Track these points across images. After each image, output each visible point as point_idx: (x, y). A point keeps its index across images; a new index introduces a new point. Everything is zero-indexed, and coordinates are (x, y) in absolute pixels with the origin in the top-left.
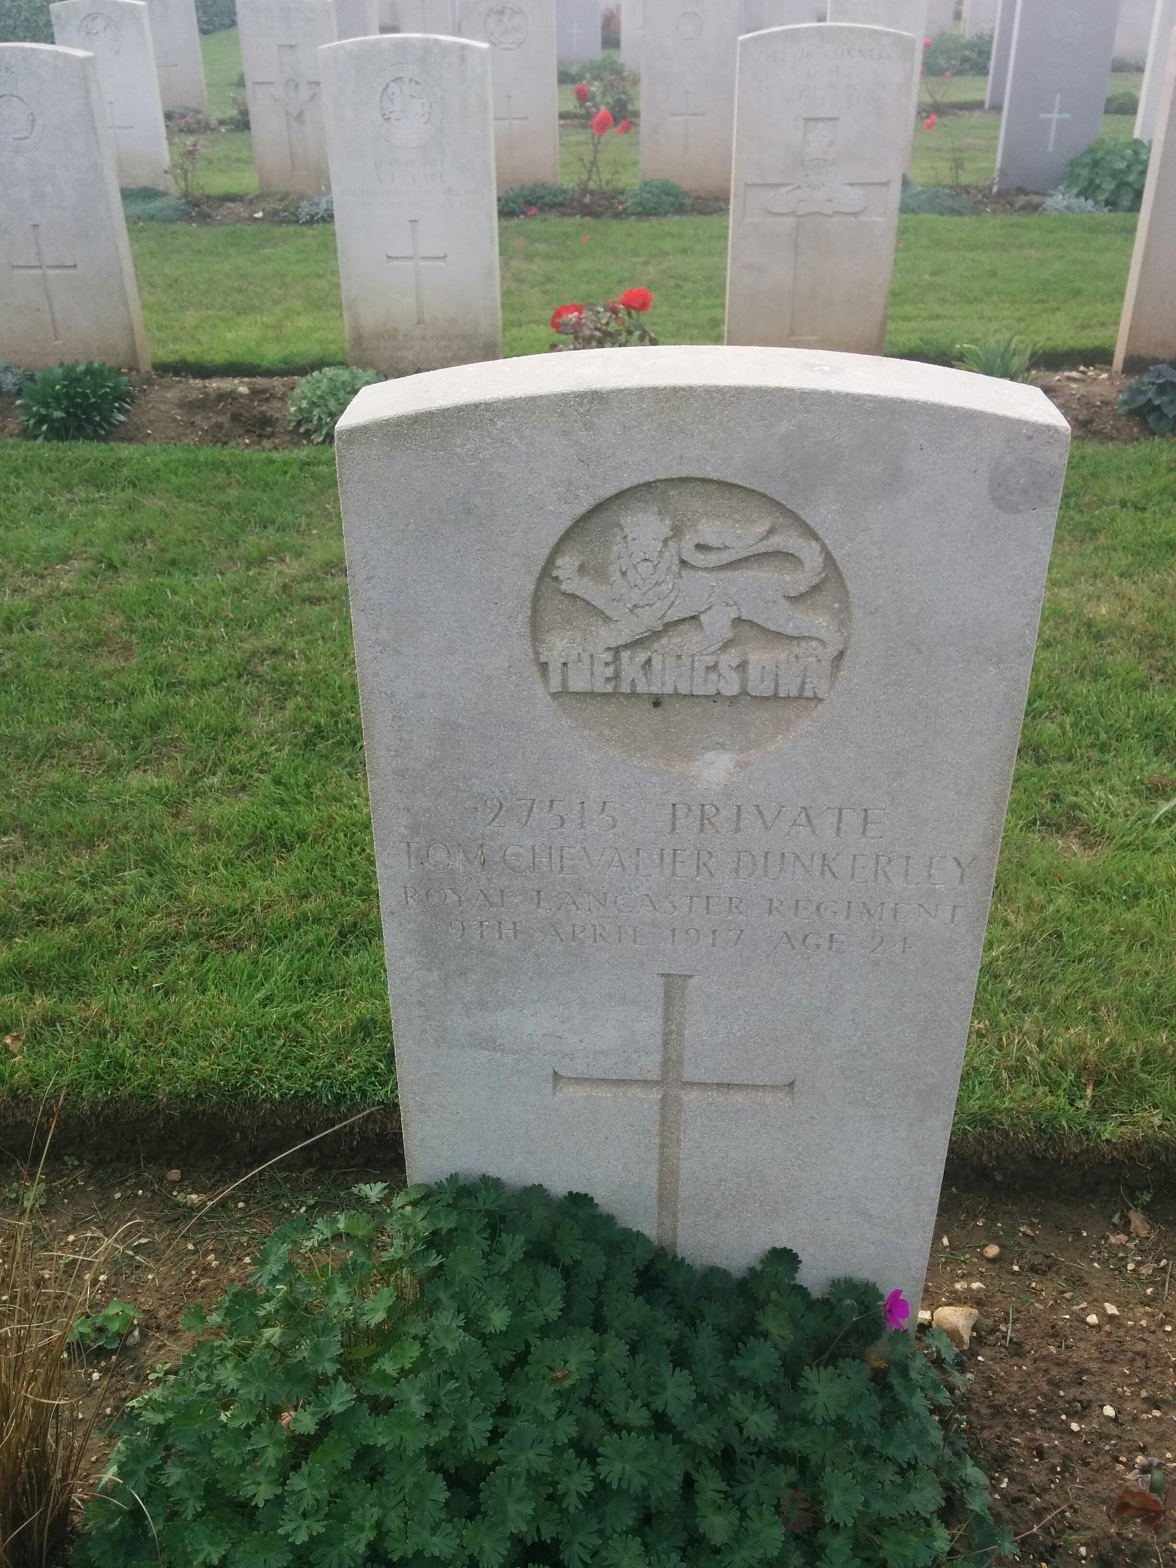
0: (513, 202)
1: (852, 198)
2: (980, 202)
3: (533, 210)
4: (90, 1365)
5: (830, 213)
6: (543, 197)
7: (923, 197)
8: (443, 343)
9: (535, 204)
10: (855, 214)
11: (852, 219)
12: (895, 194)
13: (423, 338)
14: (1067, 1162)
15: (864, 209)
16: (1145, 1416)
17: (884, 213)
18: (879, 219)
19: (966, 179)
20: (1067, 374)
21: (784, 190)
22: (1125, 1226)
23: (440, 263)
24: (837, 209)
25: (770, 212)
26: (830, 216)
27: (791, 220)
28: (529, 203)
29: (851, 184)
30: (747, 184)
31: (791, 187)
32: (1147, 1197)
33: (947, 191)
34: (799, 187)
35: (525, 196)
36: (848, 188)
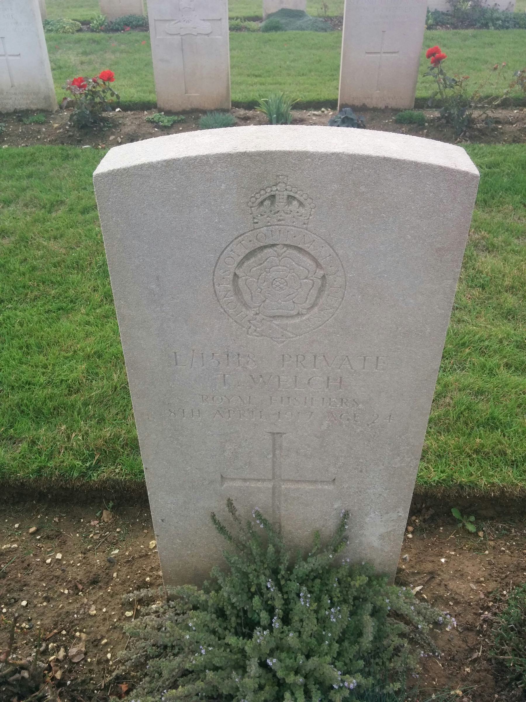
0: (119, 25)
1: (207, 27)
2: (337, 24)
3: (128, 28)
4: (75, 531)
5: (196, 34)
6: (131, 22)
7: (309, 22)
8: (25, 96)
9: (128, 26)
10: (208, 35)
11: (206, 37)
12: (226, 24)
13: (15, 94)
14: (77, 490)
15: (211, 32)
16: (39, 605)
17: (222, 32)
18: (220, 37)
19: (329, 13)
20: (313, 112)
21: (173, 22)
22: (99, 518)
23: (18, 58)
24: (199, 32)
25: (168, 33)
26: (196, 36)
27: (179, 37)
28: (126, 25)
29: (204, 20)
30: (155, 20)
31: (176, 21)
32: (111, 504)
33: (321, 19)
34: (180, 21)
35: (124, 21)
36: (203, 22)
